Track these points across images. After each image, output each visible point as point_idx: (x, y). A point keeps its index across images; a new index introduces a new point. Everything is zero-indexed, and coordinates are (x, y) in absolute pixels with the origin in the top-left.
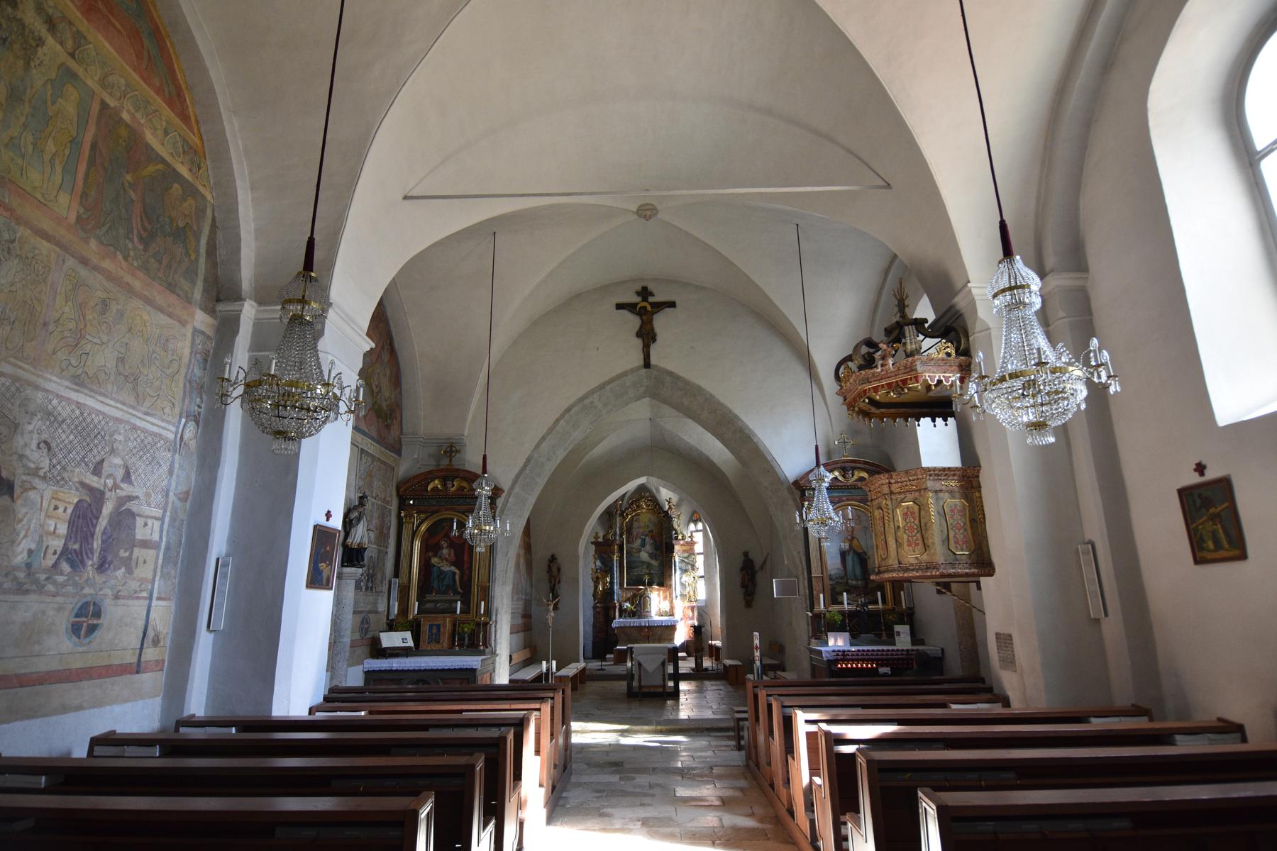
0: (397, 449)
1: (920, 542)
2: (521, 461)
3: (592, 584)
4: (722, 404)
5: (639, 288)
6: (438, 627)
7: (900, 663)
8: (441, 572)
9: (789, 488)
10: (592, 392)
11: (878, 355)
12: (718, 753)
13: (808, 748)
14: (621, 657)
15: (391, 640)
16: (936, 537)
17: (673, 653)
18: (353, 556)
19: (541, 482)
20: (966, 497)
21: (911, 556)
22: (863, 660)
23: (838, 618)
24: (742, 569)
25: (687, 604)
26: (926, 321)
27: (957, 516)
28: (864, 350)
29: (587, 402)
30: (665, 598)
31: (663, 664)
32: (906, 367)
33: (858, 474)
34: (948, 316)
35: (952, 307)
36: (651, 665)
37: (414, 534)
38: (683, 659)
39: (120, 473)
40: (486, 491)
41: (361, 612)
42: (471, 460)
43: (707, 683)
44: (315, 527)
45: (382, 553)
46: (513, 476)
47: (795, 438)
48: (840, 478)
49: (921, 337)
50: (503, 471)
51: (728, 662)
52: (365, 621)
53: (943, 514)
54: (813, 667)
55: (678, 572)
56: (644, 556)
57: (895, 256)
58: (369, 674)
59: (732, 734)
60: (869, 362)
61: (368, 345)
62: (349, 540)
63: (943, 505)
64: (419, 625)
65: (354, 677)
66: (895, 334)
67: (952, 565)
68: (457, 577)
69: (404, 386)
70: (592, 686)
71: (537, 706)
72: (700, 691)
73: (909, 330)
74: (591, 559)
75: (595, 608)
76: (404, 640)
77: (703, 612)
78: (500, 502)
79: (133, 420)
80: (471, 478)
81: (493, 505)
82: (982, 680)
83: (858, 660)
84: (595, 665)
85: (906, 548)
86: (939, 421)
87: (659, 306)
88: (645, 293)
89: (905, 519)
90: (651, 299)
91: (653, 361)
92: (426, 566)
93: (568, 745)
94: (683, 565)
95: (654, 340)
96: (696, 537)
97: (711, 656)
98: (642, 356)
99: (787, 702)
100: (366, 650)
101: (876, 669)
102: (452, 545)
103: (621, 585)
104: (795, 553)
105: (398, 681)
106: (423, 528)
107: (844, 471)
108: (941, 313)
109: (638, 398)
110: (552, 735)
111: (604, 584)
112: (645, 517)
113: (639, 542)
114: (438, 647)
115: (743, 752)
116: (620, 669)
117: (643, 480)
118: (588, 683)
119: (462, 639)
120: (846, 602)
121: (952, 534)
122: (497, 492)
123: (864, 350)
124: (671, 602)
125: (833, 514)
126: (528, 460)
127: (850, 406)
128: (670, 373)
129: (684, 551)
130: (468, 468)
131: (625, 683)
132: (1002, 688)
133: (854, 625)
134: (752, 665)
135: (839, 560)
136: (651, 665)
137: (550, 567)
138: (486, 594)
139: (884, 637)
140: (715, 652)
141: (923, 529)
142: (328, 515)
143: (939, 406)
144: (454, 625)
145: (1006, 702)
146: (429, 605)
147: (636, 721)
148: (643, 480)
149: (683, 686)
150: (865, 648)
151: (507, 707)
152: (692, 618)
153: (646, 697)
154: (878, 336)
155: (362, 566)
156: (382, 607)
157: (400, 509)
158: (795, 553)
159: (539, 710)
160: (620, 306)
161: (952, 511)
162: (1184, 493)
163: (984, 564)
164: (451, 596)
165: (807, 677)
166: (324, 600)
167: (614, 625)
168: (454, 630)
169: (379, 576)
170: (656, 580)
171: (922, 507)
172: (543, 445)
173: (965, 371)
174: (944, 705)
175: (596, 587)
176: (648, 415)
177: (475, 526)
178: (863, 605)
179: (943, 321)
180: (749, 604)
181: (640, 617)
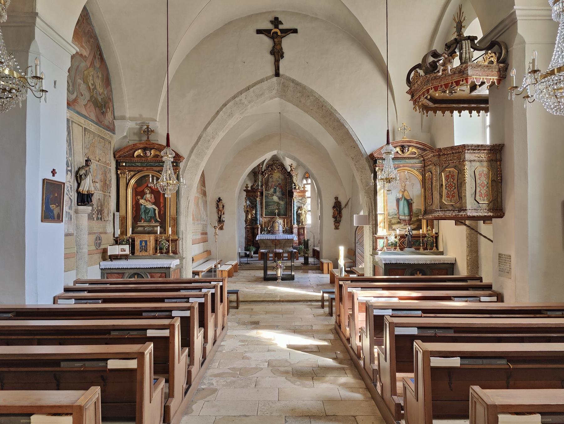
0: (112, 129)
1: (456, 195)
3: (244, 214)
6: (146, 242)
10: (241, 93)
15: (115, 250)
18: (84, 199)
24: (334, 207)
26: (476, 38)
28: (431, 59)
29: (237, 99)
40: (168, 158)
41: (95, 233)
44: (44, 180)
45: (106, 196)
48: (400, 152)
49: (472, 50)
52: (98, 239)
61: (74, 49)
62: (81, 189)
64: (133, 241)
65: (93, 273)
66: (454, 46)
68: (157, 212)
73: (466, 44)
74: (244, 200)
78: (182, 165)
80: (160, 148)
86: (474, 113)
89: (446, 180)
90: (281, 27)
91: (281, 72)
92: (137, 206)
95: (282, 57)
98: (274, 69)
100: (100, 256)
102: (153, 191)
103: (262, 215)
106: (133, 181)
111: (252, 215)
113: (272, 190)
114: (146, 254)
117: (275, 152)
122: (177, 158)
123: (431, 59)
128: (293, 81)
129: (300, 196)
130: (160, 143)
137: (218, 206)
138: (176, 222)
142: (54, 172)
145: (500, 298)
146: (139, 229)
155: (92, 205)
156: (110, 229)
157: (117, 169)
160: (259, 32)
161: (480, 175)
164: (153, 224)
167: (257, 238)
169: (106, 211)
171: (461, 172)
172: (209, 128)
175: (247, 217)
179: (489, 38)
180: (337, 228)
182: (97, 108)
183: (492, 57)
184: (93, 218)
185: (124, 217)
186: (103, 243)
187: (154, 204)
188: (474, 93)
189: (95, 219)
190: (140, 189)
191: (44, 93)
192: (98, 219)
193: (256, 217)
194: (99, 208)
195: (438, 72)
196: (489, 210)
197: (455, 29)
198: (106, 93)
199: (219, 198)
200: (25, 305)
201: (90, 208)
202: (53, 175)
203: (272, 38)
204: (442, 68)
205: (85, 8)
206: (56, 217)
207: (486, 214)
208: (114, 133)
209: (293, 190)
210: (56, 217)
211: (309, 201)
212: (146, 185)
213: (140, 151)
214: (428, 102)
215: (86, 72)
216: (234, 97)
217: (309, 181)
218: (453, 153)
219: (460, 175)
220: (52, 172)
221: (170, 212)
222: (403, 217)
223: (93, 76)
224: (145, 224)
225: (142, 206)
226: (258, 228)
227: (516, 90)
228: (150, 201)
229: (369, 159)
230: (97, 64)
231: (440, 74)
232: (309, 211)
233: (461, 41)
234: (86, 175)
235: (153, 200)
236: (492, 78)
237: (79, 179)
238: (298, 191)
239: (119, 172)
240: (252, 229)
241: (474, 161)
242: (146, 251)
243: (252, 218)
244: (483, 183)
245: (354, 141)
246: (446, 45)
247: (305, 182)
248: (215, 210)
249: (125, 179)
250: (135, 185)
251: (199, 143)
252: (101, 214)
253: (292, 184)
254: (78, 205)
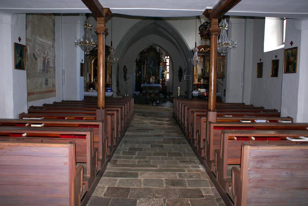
24: (179, 71)
39: (47, 54)
48: (204, 50)
56: (151, 66)
79: (47, 42)
94: (163, 69)
129: (163, 65)
135: (201, 71)
137: (124, 69)
142: (20, 39)
162: (258, 64)
193: (141, 75)
202: (20, 41)
209: (160, 62)
211: (168, 67)
217: (168, 57)
220: (21, 39)
238: (163, 62)
240: (139, 81)
243: (139, 75)
247: (166, 57)
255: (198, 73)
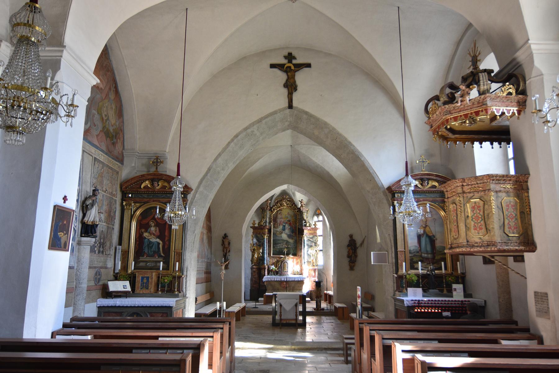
0: (120, 160)
1: (483, 227)
2: (205, 170)
3: (250, 253)
4: (340, 135)
5: (287, 54)
6: (148, 278)
7: (458, 310)
8: (150, 243)
9: (384, 192)
11: (458, 95)
12: (333, 365)
13: (404, 369)
14: (269, 300)
15: (115, 286)
16: (495, 224)
17: (303, 299)
18: (88, 230)
19: (218, 185)
20: (518, 196)
21: (476, 237)
22: (432, 307)
23: (415, 278)
24: (348, 246)
25: (311, 267)
26: (492, 71)
27: (511, 210)
28: (448, 91)
29: (249, 131)
30: (297, 263)
31: (296, 305)
32: (479, 103)
33: (432, 183)
34: (510, 66)
35: (514, 59)
36: (288, 306)
37: (132, 217)
38: (309, 302)
41: (95, 267)
42: (170, 168)
43: (324, 318)
44: (55, 206)
45: (110, 229)
46: (198, 180)
47: (388, 163)
48: (419, 186)
50: (191, 176)
51: (338, 305)
52: (98, 274)
53: (501, 208)
54: (397, 311)
55: (306, 247)
57: (470, 25)
58: (101, 309)
59: (341, 352)
60: (452, 99)
61: (95, 81)
62: (86, 219)
63: (501, 200)
65: (90, 310)
67: (506, 243)
68: (161, 246)
69: (126, 117)
70: (249, 318)
71: (211, 334)
72: (319, 323)
73: (483, 77)
74: (250, 237)
75: (252, 268)
76: (124, 287)
77: (321, 273)
78: (190, 197)
80: (169, 179)
81: (185, 199)
82: (516, 323)
83: (429, 307)
84: (251, 304)
85: (473, 231)
86: (496, 144)
87: (300, 66)
88: (290, 57)
89: (473, 211)
90: (294, 62)
91: (295, 104)
92: (140, 239)
93: (233, 359)
94: (309, 243)
95: (296, 90)
96: (318, 225)
97: (326, 300)
98: (287, 101)
99: (386, 335)
100: (99, 292)
101: (441, 313)
103: (269, 254)
104: (387, 235)
105: (120, 314)
106: (138, 213)
107: (422, 180)
108: (503, 66)
109: (284, 130)
110: (221, 353)
111: (259, 254)
112: (286, 212)
113: (281, 227)
115: (350, 366)
116: (268, 308)
117: (284, 187)
118: (247, 316)
119: (163, 287)
120: (420, 269)
121: (506, 222)
122: (187, 190)
124: (301, 266)
125: (416, 209)
126: (209, 169)
127: (435, 132)
129: (310, 234)
130: (168, 173)
131: (271, 317)
132: (537, 329)
133: (426, 283)
134: (348, 308)
136: (288, 306)
137: (223, 242)
138: (180, 257)
139: (445, 292)
140: (329, 299)
141: (486, 218)
142: (65, 199)
143: (499, 134)
144: (159, 277)
145: (541, 341)
146: (141, 264)
147: (278, 343)
148: (284, 187)
149: (309, 319)
150: (434, 299)
151: (190, 334)
152: (314, 277)
153: (286, 326)
154: (458, 82)
155: (95, 237)
156: (110, 264)
157: (123, 200)
158: (387, 235)
159: (212, 337)
160: (273, 66)
161: (508, 206)
163: (529, 243)
164: (157, 258)
165: (392, 317)
166: (62, 259)
168: (158, 280)
169: (108, 244)
170: (292, 251)
171: (486, 202)
172: (220, 159)
173: (522, 105)
174: (496, 342)
175: (253, 256)
176: (290, 143)
177: (172, 211)
178: (432, 270)
180: (352, 268)
181: (281, 275)
182: (108, 139)
183: (510, 88)
184: (95, 251)
185: (126, 251)
186: (102, 279)
187: (158, 237)
188: (494, 124)
189: (97, 251)
190: (144, 222)
191: (70, 118)
192: (99, 252)
193: (263, 257)
194: (102, 241)
195: (457, 102)
196: (520, 244)
197: (471, 63)
198: (117, 124)
199: (225, 235)
200: (22, 339)
201: (94, 240)
202: (64, 202)
203: (286, 72)
204: (460, 99)
205: (106, 45)
206: (62, 245)
207: (517, 248)
208: (122, 164)
209: (304, 228)
210: (62, 245)
212: (151, 217)
213: (147, 182)
214: (447, 132)
215: (100, 104)
216: (246, 129)
218: (477, 184)
219: (486, 206)
220: (67, 200)
221: (174, 246)
222: (426, 255)
223: (107, 107)
224: (148, 259)
225: (146, 240)
226: (265, 268)
227: (539, 113)
228: (154, 234)
229: (387, 192)
230: (112, 96)
231: (459, 104)
232: (321, 250)
233: (477, 73)
234: (92, 205)
235: (158, 233)
236: (512, 109)
237: (85, 209)
239: (124, 204)
241: (500, 191)
242: (148, 289)
243: (258, 257)
244: (511, 214)
245: (370, 173)
246: (463, 77)
248: (221, 248)
249: (130, 211)
250: (140, 217)
251: (209, 175)
252: (103, 247)
253: (302, 221)
254: (81, 236)
255: (409, 246)
